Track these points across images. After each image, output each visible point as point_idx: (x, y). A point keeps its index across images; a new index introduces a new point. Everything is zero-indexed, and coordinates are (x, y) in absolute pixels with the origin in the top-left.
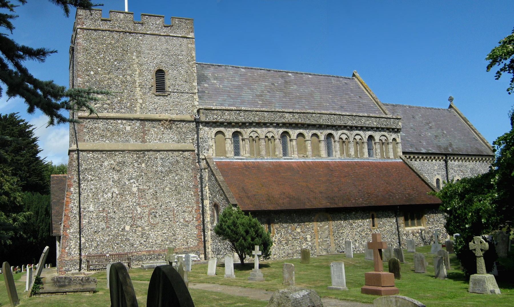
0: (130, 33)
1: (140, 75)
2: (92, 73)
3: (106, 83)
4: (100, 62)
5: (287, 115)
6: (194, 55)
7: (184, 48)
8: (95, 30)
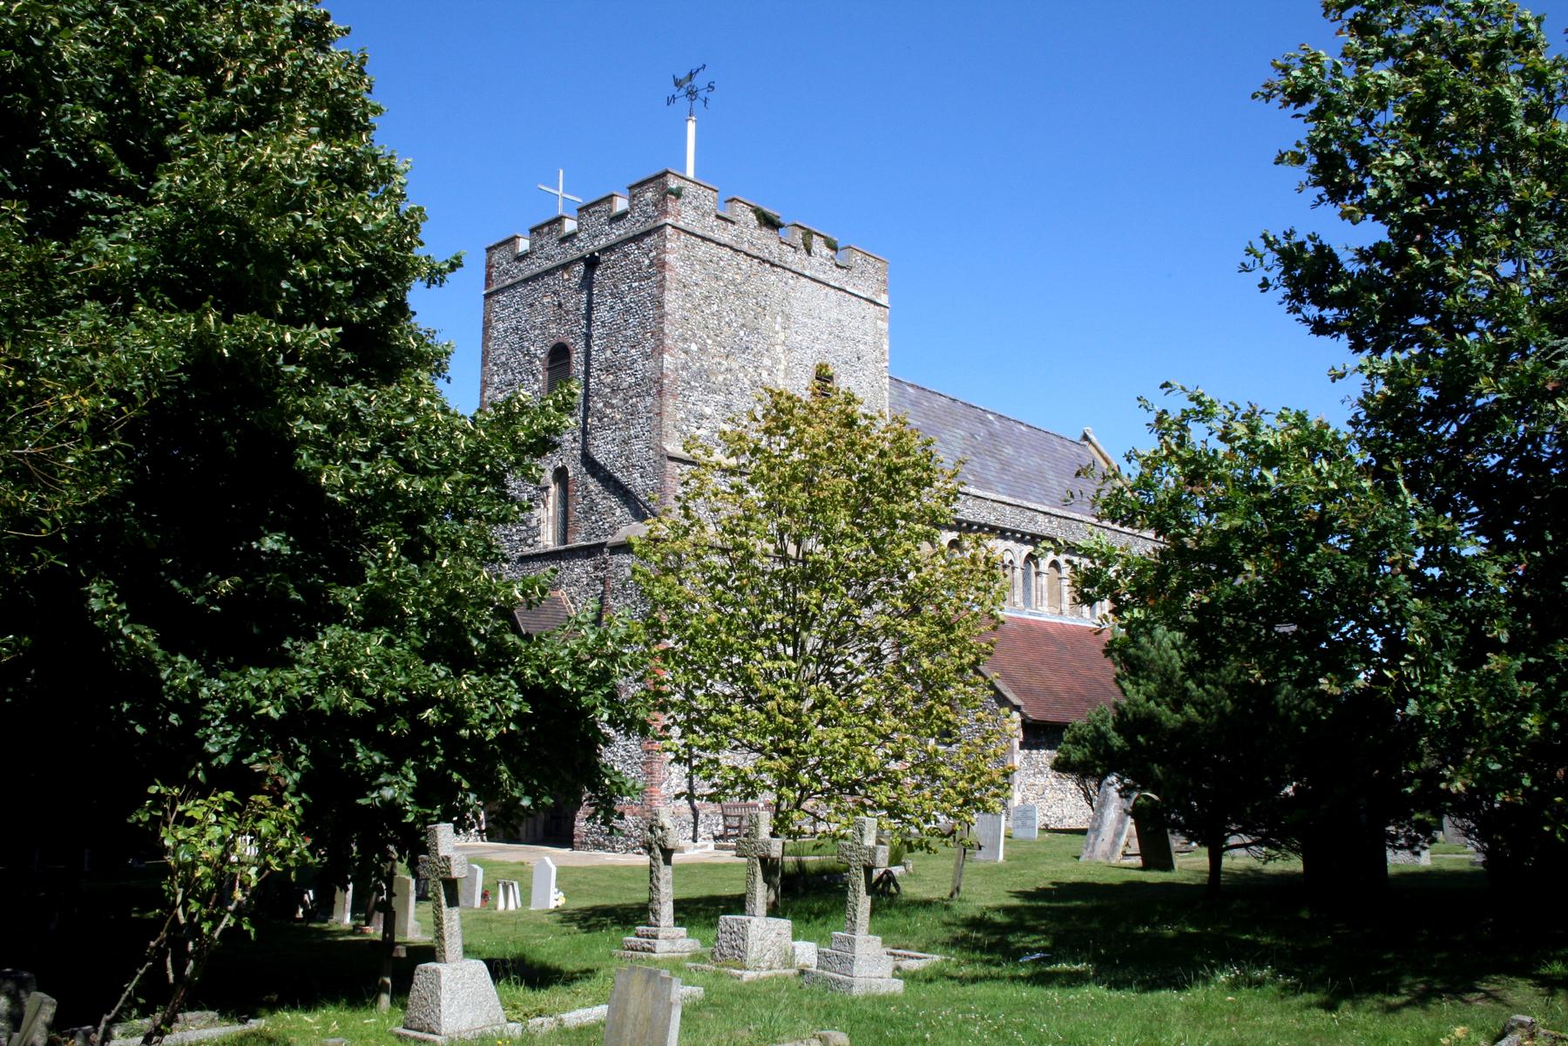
0: (772, 265)
1: (787, 371)
2: (694, 347)
3: (720, 378)
4: (713, 323)
5: (1040, 517)
6: (886, 347)
8: (704, 239)
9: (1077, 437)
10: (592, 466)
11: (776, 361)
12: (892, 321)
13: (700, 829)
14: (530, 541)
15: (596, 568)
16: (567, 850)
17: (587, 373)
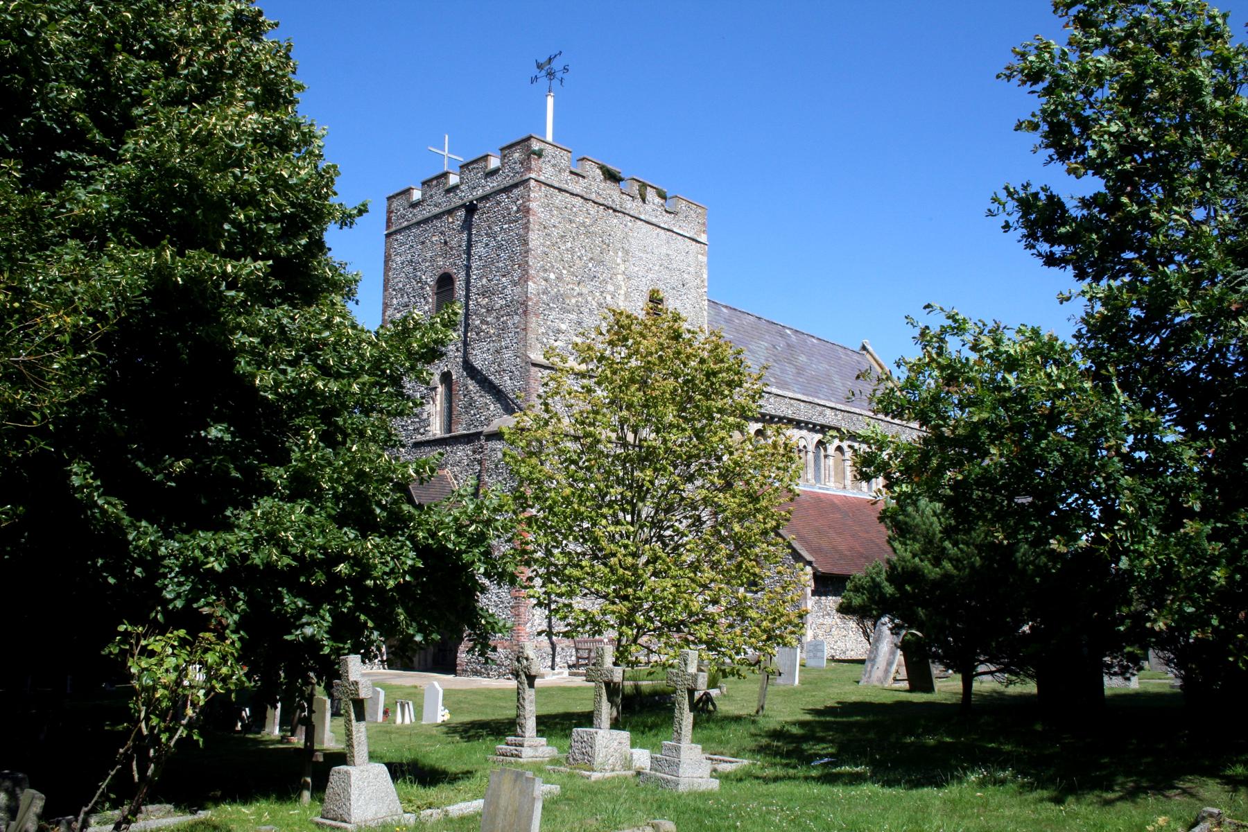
0: (615, 211)
2: (552, 276)
3: (573, 301)
4: (567, 257)
5: (828, 412)
6: (705, 276)
7: (691, 259)
8: (560, 190)
9: (857, 348)
10: (471, 371)
11: (618, 287)
12: (710, 255)
13: (557, 659)
14: (422, 430)
15: (474, 452)
16: (451, 676)
17: (467, 297)
